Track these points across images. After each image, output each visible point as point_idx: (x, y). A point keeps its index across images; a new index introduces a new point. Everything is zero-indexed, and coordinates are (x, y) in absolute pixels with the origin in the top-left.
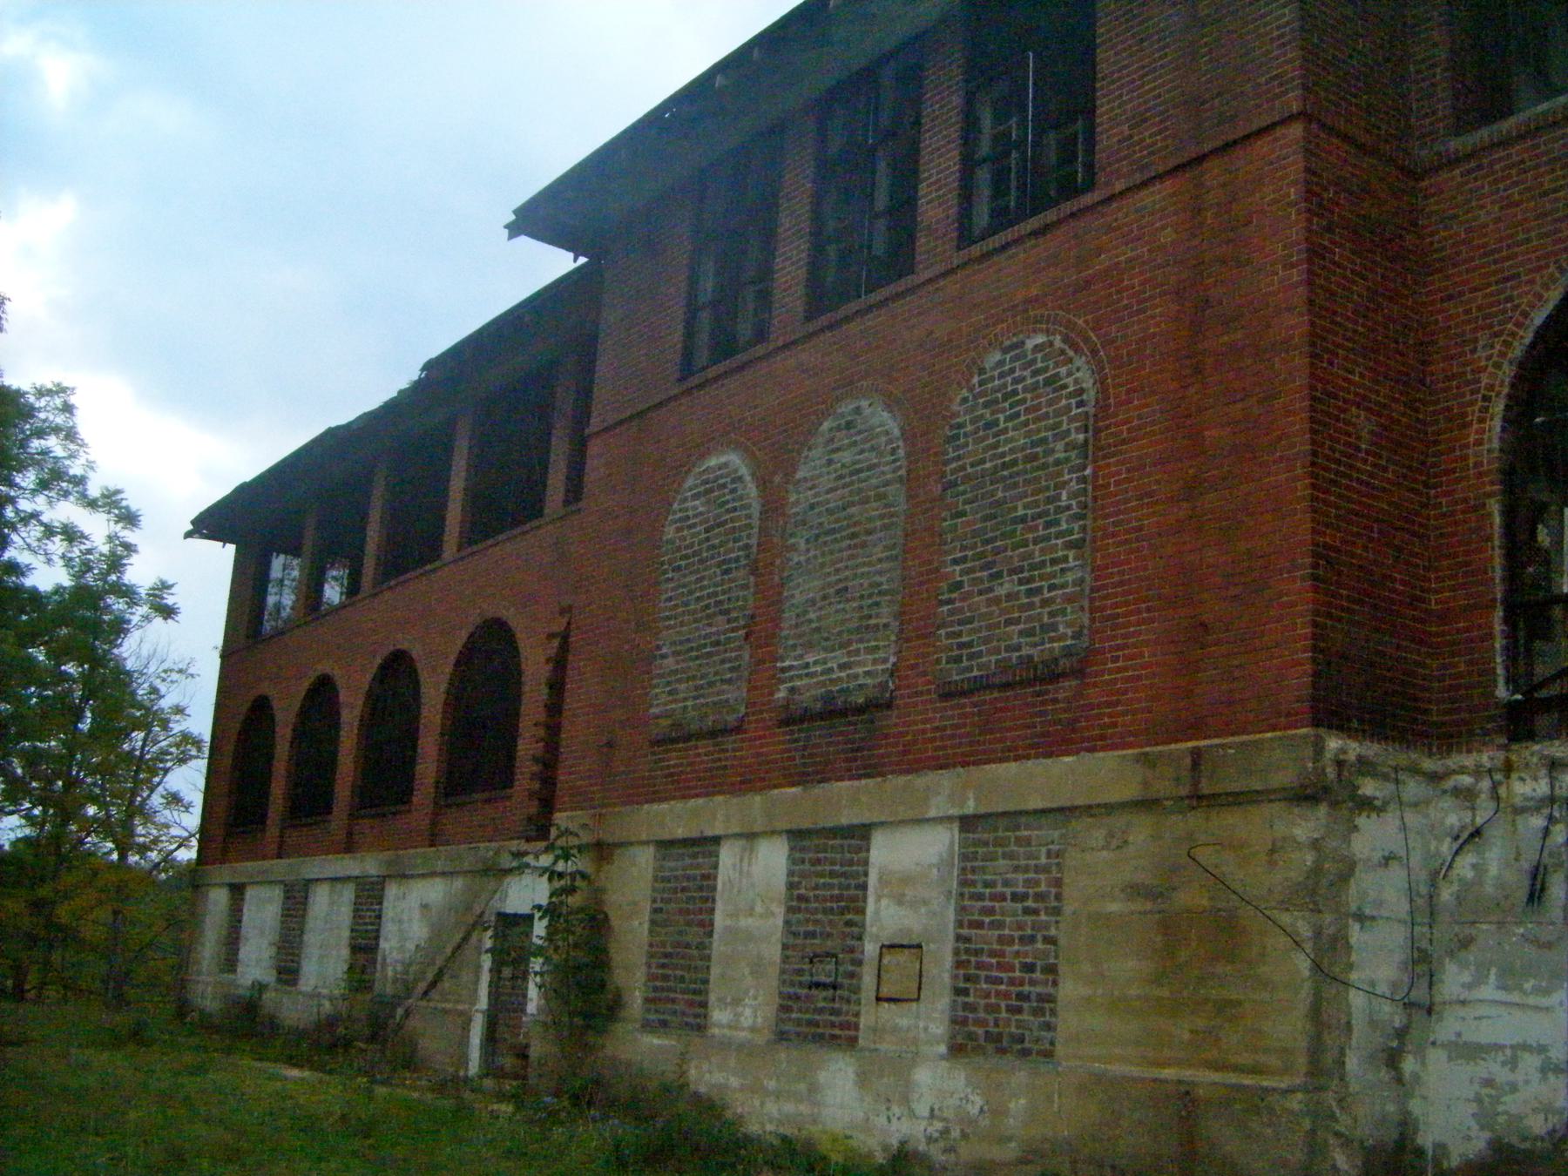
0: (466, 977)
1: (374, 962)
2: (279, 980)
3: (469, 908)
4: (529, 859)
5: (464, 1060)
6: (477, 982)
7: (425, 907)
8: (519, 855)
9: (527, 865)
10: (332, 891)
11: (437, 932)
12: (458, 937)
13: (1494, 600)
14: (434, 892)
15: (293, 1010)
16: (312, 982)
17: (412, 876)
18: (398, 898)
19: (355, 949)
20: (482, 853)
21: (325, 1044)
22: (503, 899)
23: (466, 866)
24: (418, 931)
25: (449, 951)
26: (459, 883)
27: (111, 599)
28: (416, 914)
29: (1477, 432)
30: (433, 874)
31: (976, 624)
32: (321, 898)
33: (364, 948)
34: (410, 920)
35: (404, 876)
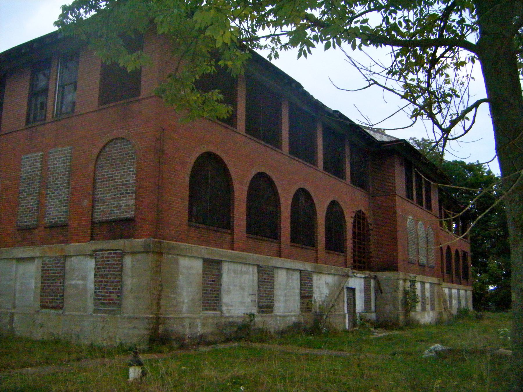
0: (341, 305)
1: (311, 301)
2: (259, 312)
3: (340, 285)
4: (355, 274)
5: (345, 326)
6: (344, 306)
7: (327, 284)
8: (354, 273)
9: (355, 276)
10: (287, 272)
11: (331, 293)
12: (337, 293)
13: (159, 242)
14: (330, 279)
15: (272, 323)
16: (282, 310)
17: (322, 273)
18: (317, 280)
19: (303, 297)
20: (344, 270)
21: (291, 333)
22: (348, 283)
23: (340, 274)
24: (326, 291)
25: (336, 297)
26: (336, 278)
27: (238, 45)
28: (324, 286)
29: (263, 186)
30: (329, 274)
31: (100, 181)
32: (281, 277)
33: (306, 296)
34: (323, 287)
35: (320, 273)
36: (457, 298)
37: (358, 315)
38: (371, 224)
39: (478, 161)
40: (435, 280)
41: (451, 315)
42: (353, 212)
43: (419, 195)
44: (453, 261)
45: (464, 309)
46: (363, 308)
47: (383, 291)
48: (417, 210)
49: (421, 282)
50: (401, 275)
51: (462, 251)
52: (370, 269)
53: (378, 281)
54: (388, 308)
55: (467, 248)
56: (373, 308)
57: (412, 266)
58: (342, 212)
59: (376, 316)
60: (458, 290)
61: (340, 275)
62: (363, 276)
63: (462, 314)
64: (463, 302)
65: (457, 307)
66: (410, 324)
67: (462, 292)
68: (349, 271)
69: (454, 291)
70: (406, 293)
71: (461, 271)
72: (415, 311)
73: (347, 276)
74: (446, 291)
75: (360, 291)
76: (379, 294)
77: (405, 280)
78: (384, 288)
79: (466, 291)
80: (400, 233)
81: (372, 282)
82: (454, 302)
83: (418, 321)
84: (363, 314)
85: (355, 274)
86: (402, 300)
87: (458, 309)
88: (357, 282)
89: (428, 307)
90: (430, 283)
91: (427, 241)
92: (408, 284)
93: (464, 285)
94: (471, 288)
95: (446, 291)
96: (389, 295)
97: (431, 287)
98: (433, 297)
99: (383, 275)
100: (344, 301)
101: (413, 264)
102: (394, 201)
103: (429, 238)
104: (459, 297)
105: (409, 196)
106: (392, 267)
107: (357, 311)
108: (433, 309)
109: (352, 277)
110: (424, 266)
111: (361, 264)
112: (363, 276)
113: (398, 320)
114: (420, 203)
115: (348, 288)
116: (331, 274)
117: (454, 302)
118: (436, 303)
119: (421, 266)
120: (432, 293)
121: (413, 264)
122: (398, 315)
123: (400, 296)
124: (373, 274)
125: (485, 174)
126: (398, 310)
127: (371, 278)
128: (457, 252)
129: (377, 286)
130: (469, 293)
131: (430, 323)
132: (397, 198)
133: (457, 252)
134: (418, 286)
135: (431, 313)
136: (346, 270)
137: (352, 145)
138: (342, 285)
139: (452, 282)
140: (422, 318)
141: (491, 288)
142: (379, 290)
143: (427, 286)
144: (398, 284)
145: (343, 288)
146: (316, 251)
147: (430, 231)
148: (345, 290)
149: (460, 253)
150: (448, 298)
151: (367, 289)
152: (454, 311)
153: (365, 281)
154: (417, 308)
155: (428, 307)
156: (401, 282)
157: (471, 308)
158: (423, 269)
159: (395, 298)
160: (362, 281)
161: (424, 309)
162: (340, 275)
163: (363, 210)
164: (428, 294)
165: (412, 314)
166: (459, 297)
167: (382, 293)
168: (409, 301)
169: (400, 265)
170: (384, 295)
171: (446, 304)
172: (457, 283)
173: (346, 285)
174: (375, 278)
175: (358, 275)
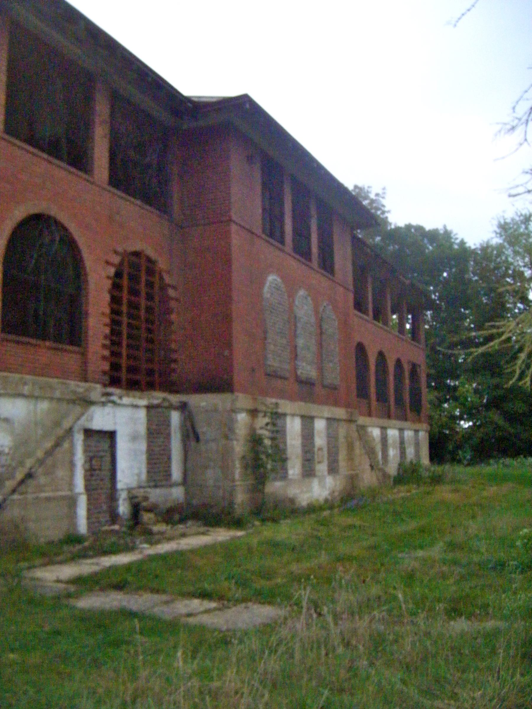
0: (61, 473)
3: (57, 424)
9: (114, 402)
12: (48, 445)
25: (40, 454)
36: (398, 445)
37: (123, 496)
38: (173, 287)
39: (445, 227)
40: (340, 413)
41: (385, 475)
42: (116, 252)
43: (301, 234)
44: (391, 378)
45: (411, 462)
46: (144, 476)
47: (201, 437)
48: (294, 265)
49: (302, 417)
50: (243, 400)
51: (409, 362)
52: (172, 387)
53: (190, 413)
54: (211, 476)
55: (416, 354)
56: (176, 474)
57: (279, 383)
58: (71, 244)
59: (187, 493)
60: (401, 430)
61: (59, 400)
62: (144, 402)
63: (408, 474)
64: (410, 452)
65: (398, 459)
66: (268, 510)
67: (408, 434)
68: (96, 391)
69: (393, 433)
70: (255, 441)
71: (407, 397)
72: (285, 477)
73: (87, 403)
74: (376, 432)
75: (134, 438)
76: (193, 444)
77: (253, 413)
78: (202, 429)
79: (416, 431)
80: (239, 306)
81: (175, 417)
82: (393, 453)
83: (292, 501)
84: (141, 493)
85: (115, 398)
86: (244, 457)
87: (400, 465)
88: (124, 417)
89: (322, 468)
90: (328, 419)
91: (321, 333)
92: (262, 421)
93: (413, 421)
94: (425, 426)
95: (376, 432)
96: (213, 445)
97: (329, 427)
98: (336, 447)
99: (200, 402)
100: (72, 465)
101: (281, 378)
102: (227, 235)
103: (325, 326)
104: (402, 442)
105: (273, 230)
106: (218, 383)
107: (120, 486)
108: (333, 470)
109: (104, 404)
110: (313, 384)
111: (128, 374)
112: (144, 402)
113: (231, 504)
114: (303, 252)
115: (88, 433)
116: (23, 396)
117: (393, 453)
118: (342, 456)
119: (308, 383)
120: (332, 438)
121: (281, 378)
122: (232, 493)
123: (239, 447)
124: (175, 399)
125: (456, 247)
126: (233, 481)
127: (171, 407)
128: (399, 363)
129: (188, 424)
130: (423, 436)
131: (326, 501)
132: (234, 228)
133: (399, 363)
134: (294, 426)
135: (329, 481)
136: (80, 387)
137: (115, 98)
138: (66, 424)
139: (389, 417)
140: (302, 492)
141: (466, 425)
142: (191, 434)
143: (320, 425)
144: (233, 421)
145: (70, 431)
146: (84, 354)
147: (329, 313)
148: (79, 439)
149: (407, 367)
150: (378, 448)
151: (157, 433)
152: (392, 469)
153: (148, 415)
154: (291, 472)
155: (322, 468)
156: (242, 417)
157: (425, 461)
158: (306, 390)
159: (226, 454)
160: (142, 414)
161: (309, 472)
162: (59, 400)
163: (150, 252)
164: (320, 441)
165: (274, 487)
166: (402, 442)
167: (198, 439)
168: (263, 459)
169: (240, 375)
170: (202, 447)
171: (376, 457)
172: (398, 418)
173: (83, 422)
174: (183, 407)
175: (126, 400)
